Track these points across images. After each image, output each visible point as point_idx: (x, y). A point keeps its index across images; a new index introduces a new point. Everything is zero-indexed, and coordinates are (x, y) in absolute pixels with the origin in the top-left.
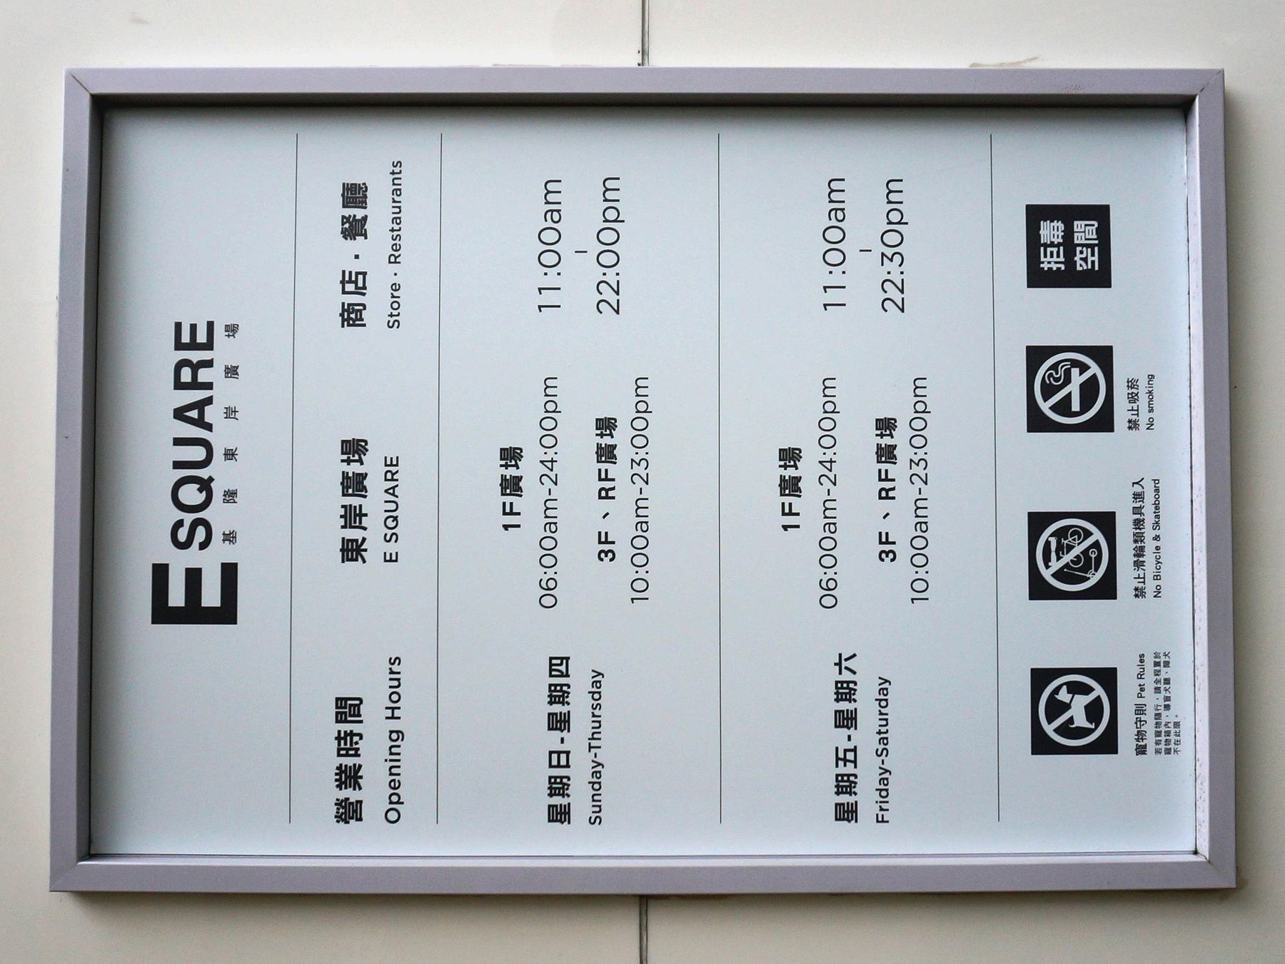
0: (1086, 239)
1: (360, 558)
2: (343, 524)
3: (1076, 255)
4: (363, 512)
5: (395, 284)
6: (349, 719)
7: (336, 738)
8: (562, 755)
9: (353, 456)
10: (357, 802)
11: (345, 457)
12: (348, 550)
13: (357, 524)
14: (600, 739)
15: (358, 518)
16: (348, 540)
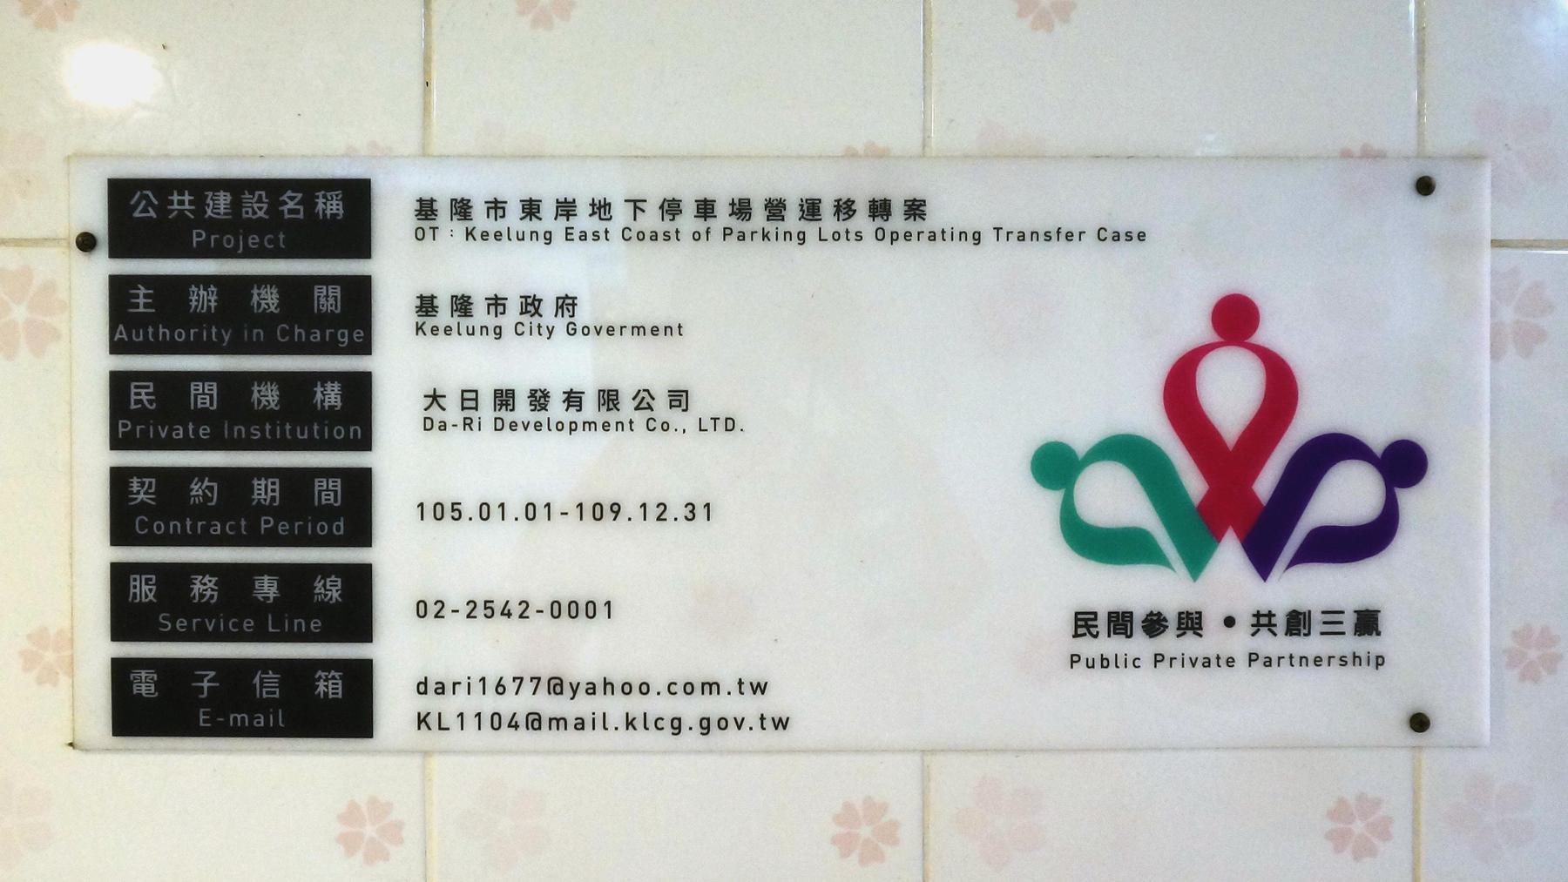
2: (560, 200)
3: (323, 671)
4: (570, 217)
5: (1145, 235)
7: (531, 198)
8: (474, 402)
10: (783, 216)
11: (736, 201)
12: (706, 205)
13: (560, 212)
14: (584, 430)
16: (713, 206)
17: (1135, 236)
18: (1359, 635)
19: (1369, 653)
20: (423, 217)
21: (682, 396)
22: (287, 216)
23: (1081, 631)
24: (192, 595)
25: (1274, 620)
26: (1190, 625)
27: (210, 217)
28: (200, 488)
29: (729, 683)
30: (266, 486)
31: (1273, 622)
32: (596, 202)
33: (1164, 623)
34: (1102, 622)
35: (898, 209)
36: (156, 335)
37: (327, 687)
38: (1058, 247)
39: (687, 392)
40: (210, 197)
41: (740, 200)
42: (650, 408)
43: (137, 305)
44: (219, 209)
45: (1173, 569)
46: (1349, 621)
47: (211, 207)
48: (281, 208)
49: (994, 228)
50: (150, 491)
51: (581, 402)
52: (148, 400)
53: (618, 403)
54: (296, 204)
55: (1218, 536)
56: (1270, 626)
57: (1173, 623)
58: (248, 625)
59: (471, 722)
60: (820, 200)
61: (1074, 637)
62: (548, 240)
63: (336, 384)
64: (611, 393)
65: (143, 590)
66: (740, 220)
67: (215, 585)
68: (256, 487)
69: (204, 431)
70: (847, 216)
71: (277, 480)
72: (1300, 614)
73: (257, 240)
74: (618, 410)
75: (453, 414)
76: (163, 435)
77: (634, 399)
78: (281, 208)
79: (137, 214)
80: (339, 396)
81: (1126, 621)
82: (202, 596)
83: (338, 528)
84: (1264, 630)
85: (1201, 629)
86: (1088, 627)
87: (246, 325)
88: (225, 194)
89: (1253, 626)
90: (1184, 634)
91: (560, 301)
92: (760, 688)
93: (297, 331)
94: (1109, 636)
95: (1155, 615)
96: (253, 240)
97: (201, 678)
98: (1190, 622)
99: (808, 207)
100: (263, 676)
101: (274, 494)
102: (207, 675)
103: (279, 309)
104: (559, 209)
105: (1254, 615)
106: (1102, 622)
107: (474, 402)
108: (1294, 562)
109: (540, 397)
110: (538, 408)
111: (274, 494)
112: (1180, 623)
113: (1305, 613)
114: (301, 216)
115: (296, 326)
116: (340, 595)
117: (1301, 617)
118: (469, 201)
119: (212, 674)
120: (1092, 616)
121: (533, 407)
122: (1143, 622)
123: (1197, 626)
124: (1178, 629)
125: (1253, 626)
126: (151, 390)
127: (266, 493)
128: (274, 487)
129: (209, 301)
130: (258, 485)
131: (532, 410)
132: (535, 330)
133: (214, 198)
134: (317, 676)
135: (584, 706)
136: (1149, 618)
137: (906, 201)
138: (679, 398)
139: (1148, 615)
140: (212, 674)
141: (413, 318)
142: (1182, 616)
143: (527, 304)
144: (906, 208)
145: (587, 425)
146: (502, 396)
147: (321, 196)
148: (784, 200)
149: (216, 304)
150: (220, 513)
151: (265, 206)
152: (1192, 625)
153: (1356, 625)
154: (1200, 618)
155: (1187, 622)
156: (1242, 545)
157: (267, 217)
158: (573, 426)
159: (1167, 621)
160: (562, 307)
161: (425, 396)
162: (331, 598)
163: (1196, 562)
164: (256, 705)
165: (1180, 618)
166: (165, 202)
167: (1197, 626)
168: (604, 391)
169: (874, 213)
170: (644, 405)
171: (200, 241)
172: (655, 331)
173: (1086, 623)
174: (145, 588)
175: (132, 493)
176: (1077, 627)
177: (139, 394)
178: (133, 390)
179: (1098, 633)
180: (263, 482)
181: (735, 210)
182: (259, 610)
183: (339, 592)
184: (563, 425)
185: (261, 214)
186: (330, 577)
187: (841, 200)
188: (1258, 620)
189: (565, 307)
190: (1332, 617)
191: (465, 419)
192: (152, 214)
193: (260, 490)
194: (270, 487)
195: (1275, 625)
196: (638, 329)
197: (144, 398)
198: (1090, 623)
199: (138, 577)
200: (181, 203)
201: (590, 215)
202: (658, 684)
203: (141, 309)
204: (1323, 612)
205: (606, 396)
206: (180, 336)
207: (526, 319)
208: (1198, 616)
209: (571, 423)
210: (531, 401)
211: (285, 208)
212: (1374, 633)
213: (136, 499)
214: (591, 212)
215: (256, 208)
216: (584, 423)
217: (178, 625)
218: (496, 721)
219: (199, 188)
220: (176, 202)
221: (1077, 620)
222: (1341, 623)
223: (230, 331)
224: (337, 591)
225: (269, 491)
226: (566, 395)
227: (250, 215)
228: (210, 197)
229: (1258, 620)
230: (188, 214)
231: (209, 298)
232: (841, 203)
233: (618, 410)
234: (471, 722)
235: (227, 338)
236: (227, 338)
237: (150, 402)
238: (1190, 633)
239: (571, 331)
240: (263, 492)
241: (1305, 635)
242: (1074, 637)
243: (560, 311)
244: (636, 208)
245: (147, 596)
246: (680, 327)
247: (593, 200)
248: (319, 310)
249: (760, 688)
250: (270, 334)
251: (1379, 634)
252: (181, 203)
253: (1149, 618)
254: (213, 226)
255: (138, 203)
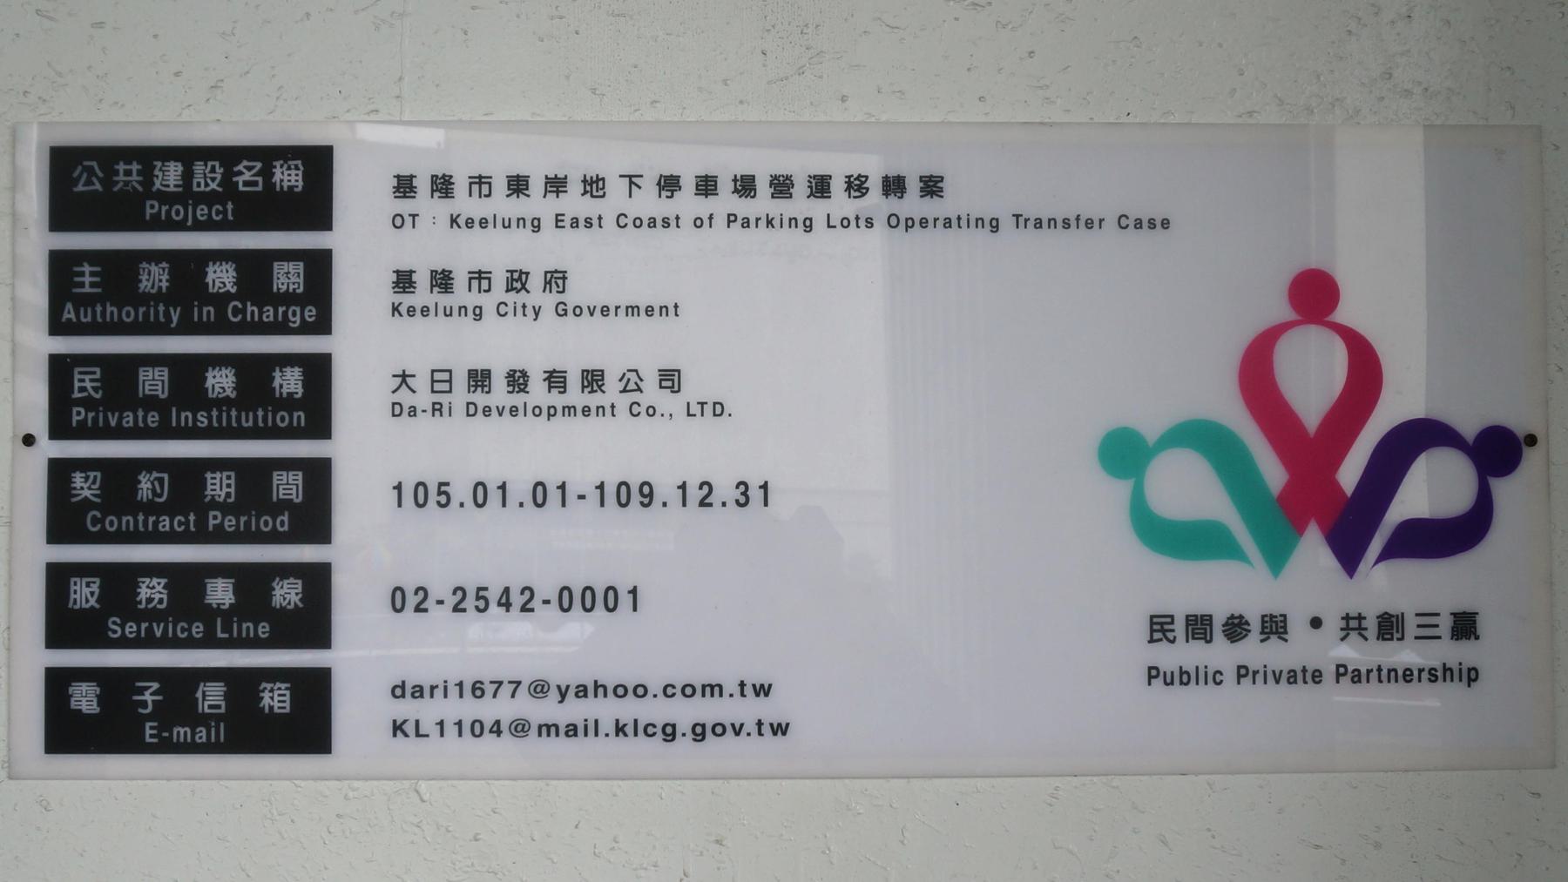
0: (278, 485)
1: (511, 192)
4: (560, 194)
5: (1169, 223)
6: (1190, 628)
8: (448, 384)
9: (740, 186)
11: (739, 177)
13: (549, 189)
15: (555, 189)
17: (1158, 223)
18: (1457, 639)
19: (1460, 664)
20: (402, 195)
21: (674, 375)
22: (241, 188)
23: (1157, 636)
24: (138, 599)
25: (1365, 624)
26: (1274, 630)
27: (158, 189)
28: (149, 480)
29: (731, 686)
30: (221, 479)
31: (1363, 626)
32: (588, 178)
33: (1246, 627)
34: (1179, 627)
35: (913, 186)
36: (103, 313)
37: (272, 698)
38: (1078, 235)
39: (679, 371)
40: (158, 167)
41: (742, 176)
42: (639, 389)
43: (82, 285)
44: (168, 180)
45: (1249, 562)
46: (1446, 624)
47: (160, 178)
48: (235, 179)
49: (1014, 215)
50: (93, 487)
51: (565, 382)
52: (93, 387)
53: (603, 384)
54: (254, 175)
55: (1300, 529)
56: (1361, 630)
57: (1255, 626)
58: (198, 629)
59: (451, 730)
60: (830, 177)
61: (1149, 642)
62: (537, 228)
63: (297, 369)
64: (595, 373)
65: (84, 594)
66: (743, 198)
67: (164, 588)
68: (209, 481)
69: (153, 419)
70: (859, 194)
71: (233, 474)
72: (1392, 616)
73: (206, 211)
74: (604, 392)
75: (423, 398)
76: (113, 423)
77: (620, 380)
78: (235, 179)
79: (80, 188)
80: (300, 383)
81: (1205, 625)
82: (150, 600)
83: (282, 523)
84: (1354, 635)
85: (1286, 632)
86: (1164, 631)
87: (196, 303)
88: (176, 164)
89: (1342, 629)
90: (1268, 638)
91: (549, 276)
92: (763, 690)
93: (249, 309)
94: (1187, 641)
95: (1236, 618)
96: (202, 212)
97: (141, 691)
98: (1274, 625)
99: (816, 183)
100: (205, 689)
101: (229, 490)
102: (150, 687)
103: (235, 287)
104: (548, 185)
105: (1343, 618)
106: (1179, 627)
107: (448, 384)
108: (1382, 557)
109: (519, 377)
110: (517, 389)
111: (229, 490)
112: (1263, 627)
113: (1397, 616)
114: (260, 188)
115: (249, 304)
116: (301, 600)
117: (1394, 620)
118: (451, 177)
119: (155, 686)
120: (1169, 620)
121: (511, 389)
122: (1223, 626)
123: (1282, 630)
124: (1261, 633)
125: (1342, 629)
126: (98, 376)
127: (221, 490)
128: (229, 482)
129: (160, 281)
130: (212, 478)
131: (509, 392)
132: (520, 310)
133: (164, 168)
134: (261, 688)
135: (575, 710)
136: (1230, 621)
137: (921, 177)
138: (670, 379)
139: (1228, 618)
140: (155, 686)
141: (388, 296)
142: (1266, 619)
143: (513, 280)
144: (922, 185)
145: (566, 410)
146: (477, 377)
147: (278, 167)
148: (791, 176)
149: (167, 284)
150: (170, 509)
151: (219, 177)
152: (1277, 628)
153: (1453, 628)
154: (1285, 621)
155: (1271, 626)
156: (1326, 538)
157: (220, 189)
158: (552, 411)
159: (1249, 625)
160: (550, 283)
161: (394, 376)
162: (289, 603)
163: (1277, 557)
164: (198, 720)
165: (1263, 622)
166: (110, 172)
167: (1282, 630)
168: (588, 371)
169: (887, 191)
170: (632, 386)
171: (154, 214)
172: (649, 311)
173: (1162, 627)
174: (86, 591)
175: (75, 488)
176: (1152, 631)
177: (83, 381)
178: (77, 377)
179: (1175, 638)
180: (218, 475)
181: (738, 187)
182: (209, 614)
183: (300, 596)
184: (540, 409)
185: (213, 186)
186: (288, 579)
187: (852, 176)
188: (1348, 624)
189: (553, 280)
190: (1427, 618)
191: (434, 404)
192: (98, 187)
193: (215, 484)
194: (225, 482)
195: (1366, 629)
196: (632, 310)
197: (88, 385)
198: (1166, 627)
199: (78, 580)
200: (128, 175)
201: (583, 195)
202: (655, 687)
203: (87, 289)
204: (1417, 615)
205: (589, 378)
206: (129, 314)
207: (511, 298)
208: (1282, 618)
209: (549, 408)
210: (508, 381)
211: (240, 179)
212: (1473, 637)
213: (80, 495)
214: (582, 192)
215: (207, 178)
216: (564, 408)
217: (127, 630)
218: (477, 729)
219: (149, 156)
220: (121, 172)
221: (1152, 623)
222: (1437, 626)
223: (179, 309)
224: (297, 594)
225: (224, 485)
226: (547, 382)
227: (202, 188)
228: (158, 167)
229: (1348, 624)
230: (137, 186)
231: (161, 277)
232: (852, 179)
233: (604, 392)
234: (451, 730)
235: (175, 319)
236: (175, 319)
237: (94, 388)
238: (1274, 638)
239: (561, 311)
240: (218, 487)
241: (1398, 639)
242: (1149, 642)
243: (548, 286)
244: (631, 183)
245: (87, 601)
246: (676, 306)
247: (585, 176)
248: (278, 289)
249: (763, 690)
250: (221, 313)
251: (1477, 638)
252: (128, 173)
253: (1230, 621)
254: (165, 198)
255: (80, 176)
